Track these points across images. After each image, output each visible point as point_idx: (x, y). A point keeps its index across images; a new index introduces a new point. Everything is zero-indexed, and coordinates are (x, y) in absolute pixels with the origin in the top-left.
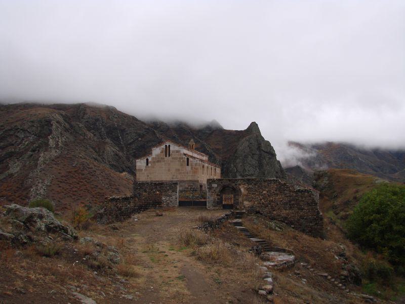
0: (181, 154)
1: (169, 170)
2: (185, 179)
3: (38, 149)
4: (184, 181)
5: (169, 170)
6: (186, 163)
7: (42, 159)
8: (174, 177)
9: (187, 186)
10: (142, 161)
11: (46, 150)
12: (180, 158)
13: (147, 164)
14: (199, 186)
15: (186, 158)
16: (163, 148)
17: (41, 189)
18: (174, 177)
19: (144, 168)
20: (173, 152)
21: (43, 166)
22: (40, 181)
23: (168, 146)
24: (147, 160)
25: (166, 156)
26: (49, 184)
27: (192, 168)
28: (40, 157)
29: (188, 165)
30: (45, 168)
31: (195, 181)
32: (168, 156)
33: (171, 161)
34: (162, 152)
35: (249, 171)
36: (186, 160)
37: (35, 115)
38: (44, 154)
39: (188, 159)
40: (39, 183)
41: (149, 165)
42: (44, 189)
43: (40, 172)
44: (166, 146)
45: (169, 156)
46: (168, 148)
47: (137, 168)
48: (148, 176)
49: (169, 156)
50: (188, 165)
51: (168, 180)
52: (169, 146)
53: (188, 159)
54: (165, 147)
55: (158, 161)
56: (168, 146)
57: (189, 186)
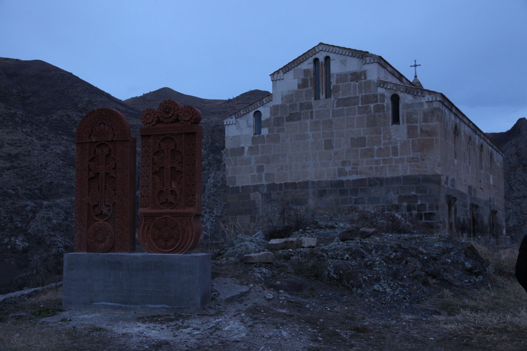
0: (368, 84)
1: (329, 145)
2: (389, 174)
3: (208, 167)
4: (380, 182)
5: (329, 145)
6: (390, 113)
7: (212, 181)
8: (348, 169)
9: (393, 197)
10: (242, 122)
11: (219, 169)
12: (367, 100)
13: (258, 131)
14: (443, 201)
15: (388, 95)
16: (306, 72)
17: (207, 221)
18: (348, 169)
19: (247, 145)
20: (342, 78)
21: (213, 190)
22: (208, 210)
23: (322, 59)
24: (258, 114)
25: (317, 98)
26: (219, 214)
27: (411, 131)
28: (209, 178)
29: (396, 120)
30: (215, 192)
31: (427, 179)
32: (323, 96)
33: (335, 114)
34: (303, 85)
35: (519, 190)
36: (388, 102)
37: (205, 124)
38: (215, 174)
39: (395, 99)
40: (205, 213)
41: (265, 131)
42: (212, 222)
43: (208, 198)
44: (316, 60)
45: (328, 96)
46: (322, 69)
47: (228, 145)
48: (260, 169)
49: (328, 96)
50: (396, 120)
51: (326, 178)
52: (327, 58)
53: (395, 99)
54: (311, 67)
55: (291, 118)
56: (322, 59)
57: (402, 199)
